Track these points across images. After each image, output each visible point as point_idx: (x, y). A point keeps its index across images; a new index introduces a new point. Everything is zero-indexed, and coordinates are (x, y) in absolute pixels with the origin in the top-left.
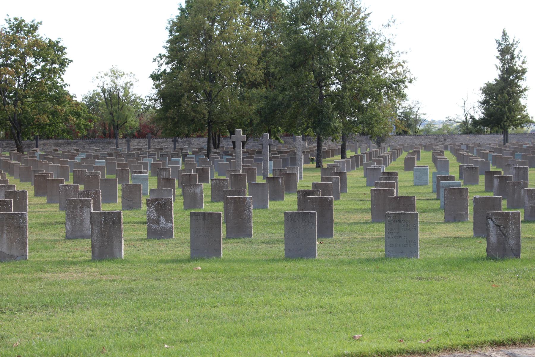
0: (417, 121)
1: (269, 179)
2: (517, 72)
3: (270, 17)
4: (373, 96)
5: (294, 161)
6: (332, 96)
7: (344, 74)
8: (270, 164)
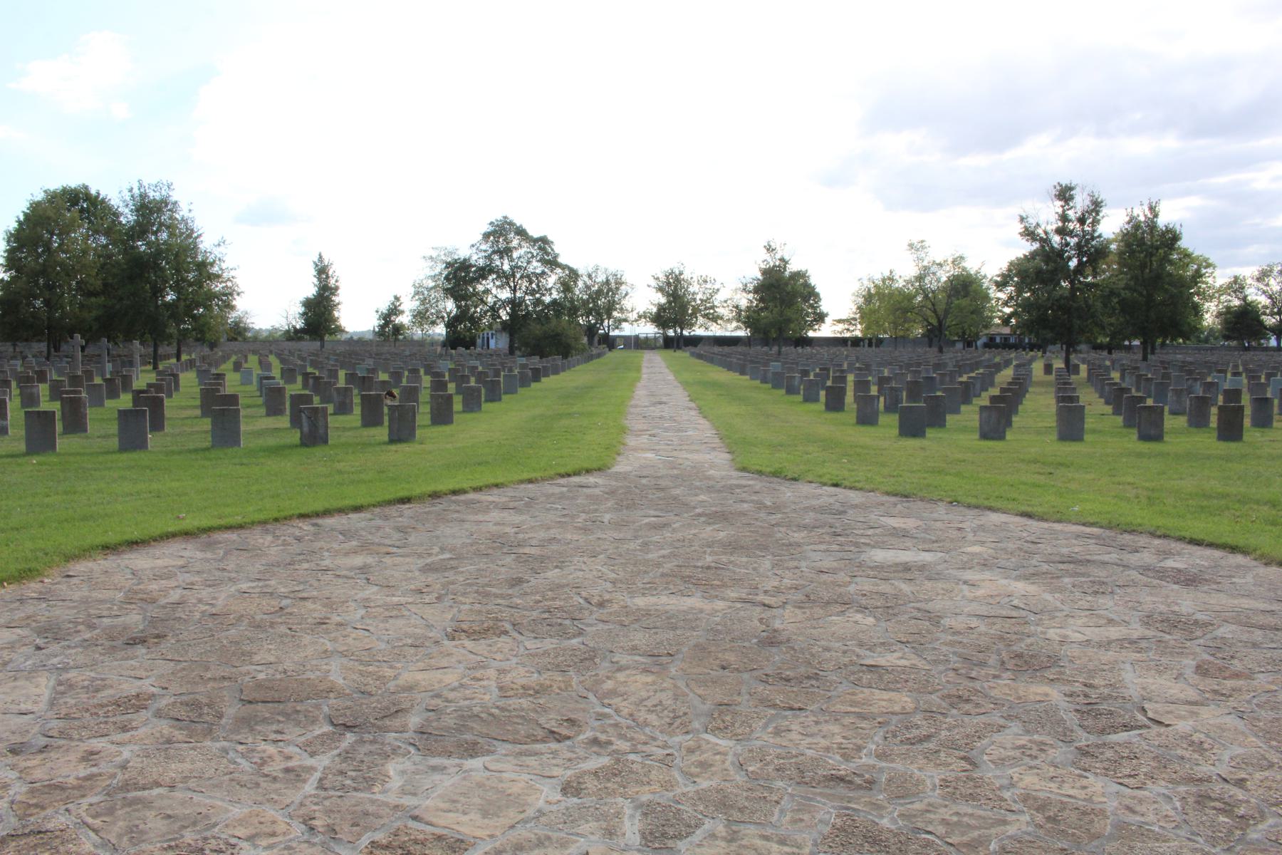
0: (246, 329)
1: (105, 380)
2: (331, 289)
3: (107, 233)
4: (205, 307)
5: (131, 364)
6: (168, 306)
7: (177, 288)
8: (109, 367)
